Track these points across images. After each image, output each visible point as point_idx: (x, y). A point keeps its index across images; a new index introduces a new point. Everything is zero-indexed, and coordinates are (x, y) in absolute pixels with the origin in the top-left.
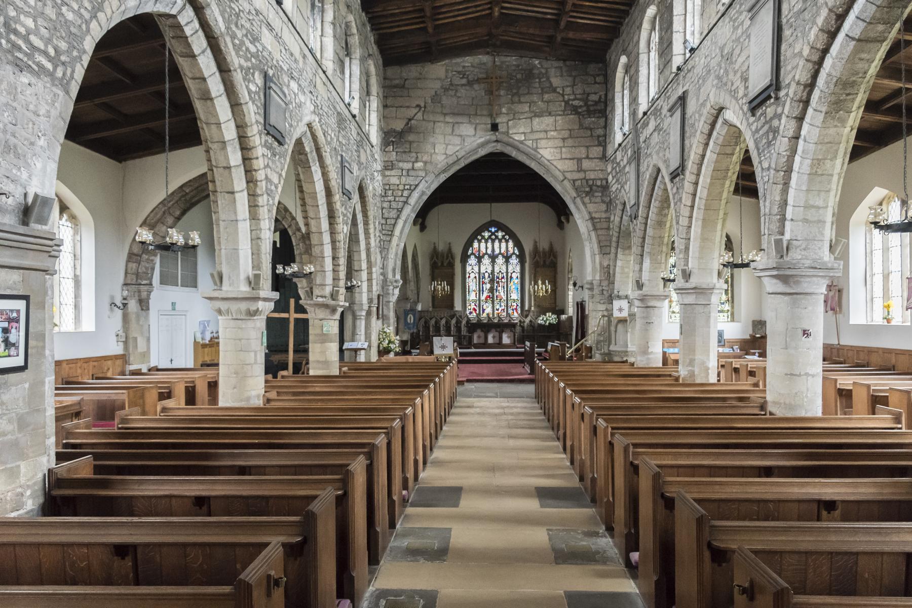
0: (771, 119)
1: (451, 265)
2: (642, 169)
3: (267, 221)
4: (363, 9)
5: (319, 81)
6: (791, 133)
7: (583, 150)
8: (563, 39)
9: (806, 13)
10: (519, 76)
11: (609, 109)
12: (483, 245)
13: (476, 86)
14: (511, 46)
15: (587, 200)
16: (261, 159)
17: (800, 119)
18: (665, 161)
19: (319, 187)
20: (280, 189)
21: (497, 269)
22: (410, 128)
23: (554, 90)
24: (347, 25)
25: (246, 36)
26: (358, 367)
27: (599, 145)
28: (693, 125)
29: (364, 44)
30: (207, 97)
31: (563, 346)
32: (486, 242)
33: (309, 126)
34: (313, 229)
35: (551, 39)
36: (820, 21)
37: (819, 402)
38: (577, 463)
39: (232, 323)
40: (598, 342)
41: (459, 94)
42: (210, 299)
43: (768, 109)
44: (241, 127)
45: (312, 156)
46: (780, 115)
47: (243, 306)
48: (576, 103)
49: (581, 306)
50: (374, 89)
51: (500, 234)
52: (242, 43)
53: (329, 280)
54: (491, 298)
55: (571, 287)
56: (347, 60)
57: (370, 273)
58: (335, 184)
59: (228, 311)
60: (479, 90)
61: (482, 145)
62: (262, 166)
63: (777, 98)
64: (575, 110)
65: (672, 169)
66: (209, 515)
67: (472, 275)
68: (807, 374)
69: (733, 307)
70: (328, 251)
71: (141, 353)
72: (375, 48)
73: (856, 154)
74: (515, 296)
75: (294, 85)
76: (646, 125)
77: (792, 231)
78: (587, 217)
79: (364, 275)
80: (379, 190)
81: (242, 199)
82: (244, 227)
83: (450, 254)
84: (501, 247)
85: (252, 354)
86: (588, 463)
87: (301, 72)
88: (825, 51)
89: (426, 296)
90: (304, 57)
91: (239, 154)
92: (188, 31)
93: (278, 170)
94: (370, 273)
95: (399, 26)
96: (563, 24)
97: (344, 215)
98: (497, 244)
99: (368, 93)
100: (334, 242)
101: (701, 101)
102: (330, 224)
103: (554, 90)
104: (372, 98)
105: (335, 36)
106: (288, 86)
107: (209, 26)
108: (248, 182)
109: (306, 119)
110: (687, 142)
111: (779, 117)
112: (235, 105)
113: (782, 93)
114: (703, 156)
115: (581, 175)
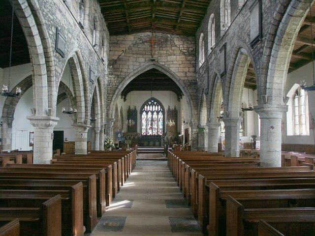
0: (259, 49)
1: (136, 115)
2: (210, 75)
3: (55, 88)
4: (102, 12)
5: (81, 36)
6: (267, 54)
7: (187, 69)
8: (179, 27)
9: (272, 7)
10: (162, 40)
11: (197, 53)
12: (148, 107)
13: (146, 44)
14: (159, 29)
15: (188, 88)
16: (53, 62)
17: (271, 48)
18: (218, 71)
19: (80, 77)
20: (61, 75)
21: (154, 117)
22: (119, 59)
23: (176, 46)
24: (95, 18)
25: (49, 12)
26: (94, 152)
27: (193, 67)
28: (229, 55)
29: (102, 26)
30: (31, 35)
31: (179, 146)
32: (150, 106)
33: (76, 52)
34: (77, 95)
35: (174, 27)
36: (277, 9)
37: (280, 163)
38: (183, 190)
39: (39, 130)
40: (193, 144)
41: (139, 46)
42: (30, 119)
43: (258, 46)
44: (45, 48)
45: (78, 66)
46: (263, 47)
47: (44, 123)
48: (184, 51)
49: (186, 131)
50: (106, 43)
51: (155, 103)
52: (47, 14)
53: (83, 116)
54: (151, 128)
55: (183, 124)
56: (94, 32)
57: (102, 115)
58: (87, 77)
59: (37, 125)
60: (147, 45)
61: (148, 66)
62: (53, 65)
63: (262, 41)
64: (184, 53)
65: (221, 72)
66: (7, 207)
67: (144, 119)
68: (276, 151)
69: (244, 130)
70: (83, 104)
71: (8, 145)
72: (106, 28)
73: (290, 71)
74: (161, 127)
75: (70, 35)
76: (211, 58)
77: (269, 93)
78: (189, 94)
79: (99, 116)
80: (106, 83)
81: (45, 78)
82: (45, 89)
83: (135, 111)
84: (155, 108)
85: (47, 143)
86: (187, 189)
87: (73, 31)
88: (280, 21)
89: (125, 127)
90: (75, 25)
91: (44, 59)
92: (23, 7)
93: (61, 67)
94: (102, 115)
95: (116, 20)
96: (179, 21)
97: (90, 90)
98: (154, 107)
99: (103, 45)
100: (86, 101)
101: (232, 46)
102: (84, 93)
103: (176, 46)
104: (105, 47)
105: (89, 20)
106: (67, 35)
107: (32, 5)
108: (47, 71)
109: (75, 49)
110: (227, 62)
111: (262, 48)
112: (43, 39)
113: (263, 39)
114: (233, 67)
115: (186, 78)
